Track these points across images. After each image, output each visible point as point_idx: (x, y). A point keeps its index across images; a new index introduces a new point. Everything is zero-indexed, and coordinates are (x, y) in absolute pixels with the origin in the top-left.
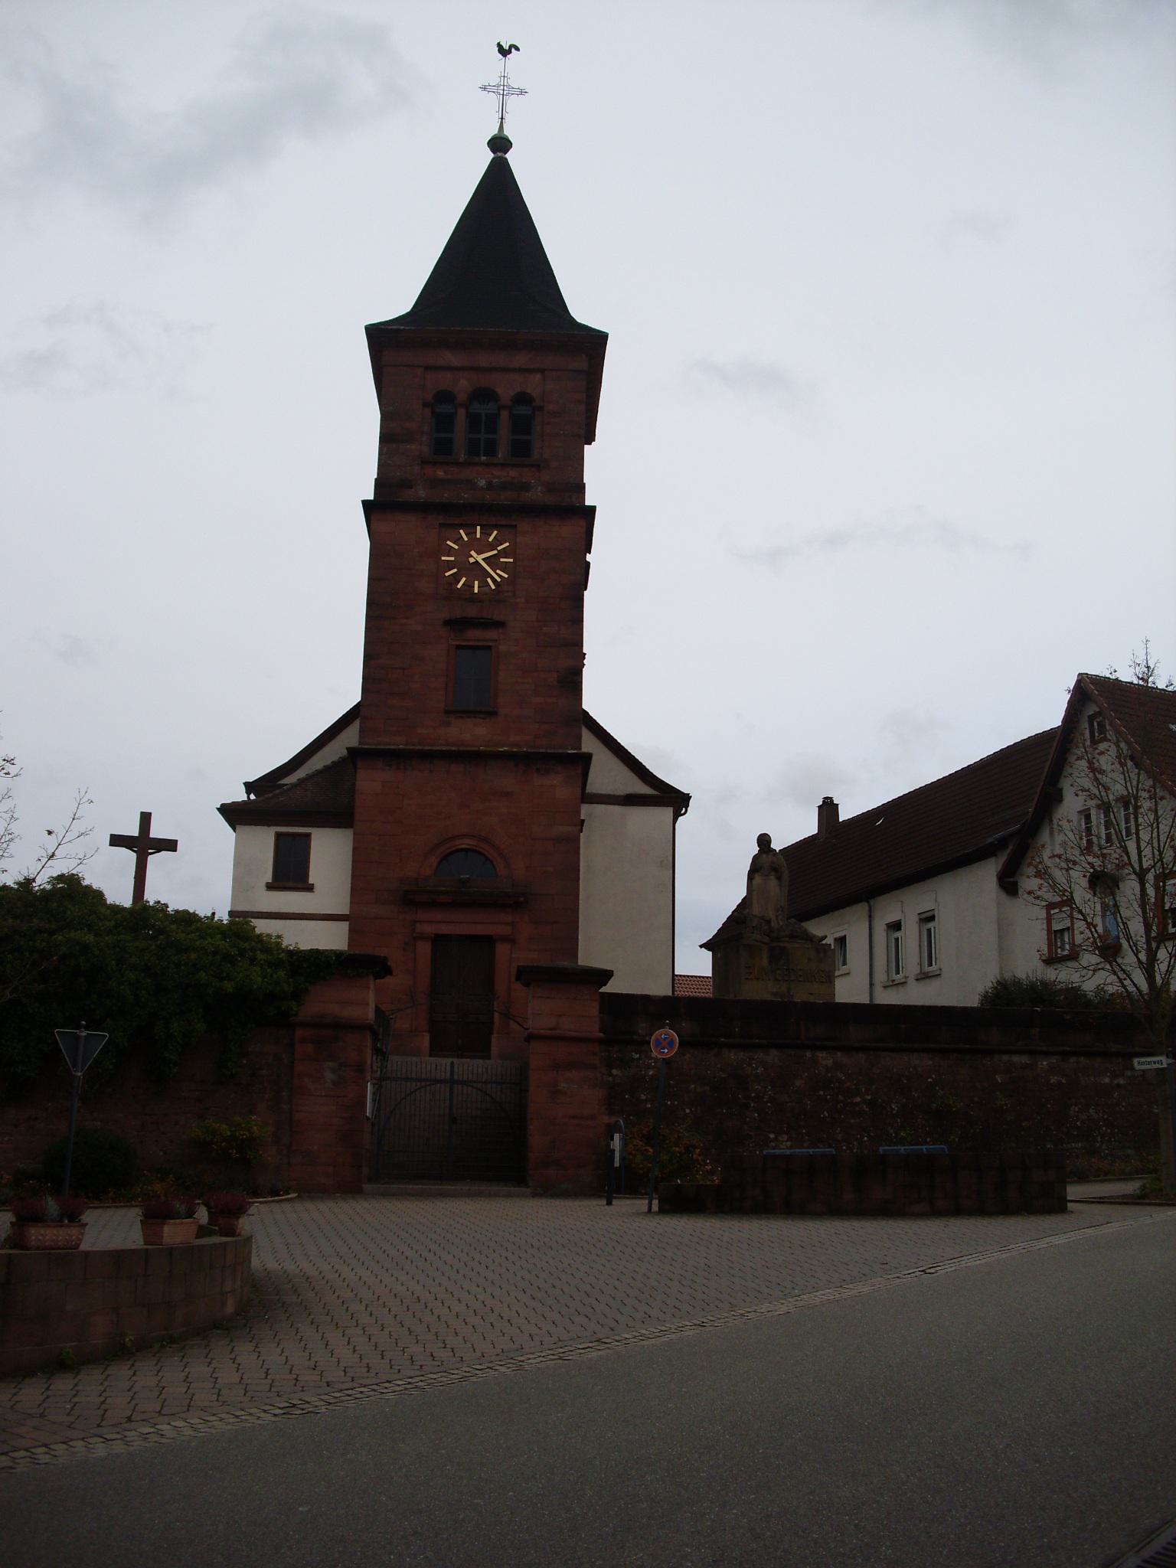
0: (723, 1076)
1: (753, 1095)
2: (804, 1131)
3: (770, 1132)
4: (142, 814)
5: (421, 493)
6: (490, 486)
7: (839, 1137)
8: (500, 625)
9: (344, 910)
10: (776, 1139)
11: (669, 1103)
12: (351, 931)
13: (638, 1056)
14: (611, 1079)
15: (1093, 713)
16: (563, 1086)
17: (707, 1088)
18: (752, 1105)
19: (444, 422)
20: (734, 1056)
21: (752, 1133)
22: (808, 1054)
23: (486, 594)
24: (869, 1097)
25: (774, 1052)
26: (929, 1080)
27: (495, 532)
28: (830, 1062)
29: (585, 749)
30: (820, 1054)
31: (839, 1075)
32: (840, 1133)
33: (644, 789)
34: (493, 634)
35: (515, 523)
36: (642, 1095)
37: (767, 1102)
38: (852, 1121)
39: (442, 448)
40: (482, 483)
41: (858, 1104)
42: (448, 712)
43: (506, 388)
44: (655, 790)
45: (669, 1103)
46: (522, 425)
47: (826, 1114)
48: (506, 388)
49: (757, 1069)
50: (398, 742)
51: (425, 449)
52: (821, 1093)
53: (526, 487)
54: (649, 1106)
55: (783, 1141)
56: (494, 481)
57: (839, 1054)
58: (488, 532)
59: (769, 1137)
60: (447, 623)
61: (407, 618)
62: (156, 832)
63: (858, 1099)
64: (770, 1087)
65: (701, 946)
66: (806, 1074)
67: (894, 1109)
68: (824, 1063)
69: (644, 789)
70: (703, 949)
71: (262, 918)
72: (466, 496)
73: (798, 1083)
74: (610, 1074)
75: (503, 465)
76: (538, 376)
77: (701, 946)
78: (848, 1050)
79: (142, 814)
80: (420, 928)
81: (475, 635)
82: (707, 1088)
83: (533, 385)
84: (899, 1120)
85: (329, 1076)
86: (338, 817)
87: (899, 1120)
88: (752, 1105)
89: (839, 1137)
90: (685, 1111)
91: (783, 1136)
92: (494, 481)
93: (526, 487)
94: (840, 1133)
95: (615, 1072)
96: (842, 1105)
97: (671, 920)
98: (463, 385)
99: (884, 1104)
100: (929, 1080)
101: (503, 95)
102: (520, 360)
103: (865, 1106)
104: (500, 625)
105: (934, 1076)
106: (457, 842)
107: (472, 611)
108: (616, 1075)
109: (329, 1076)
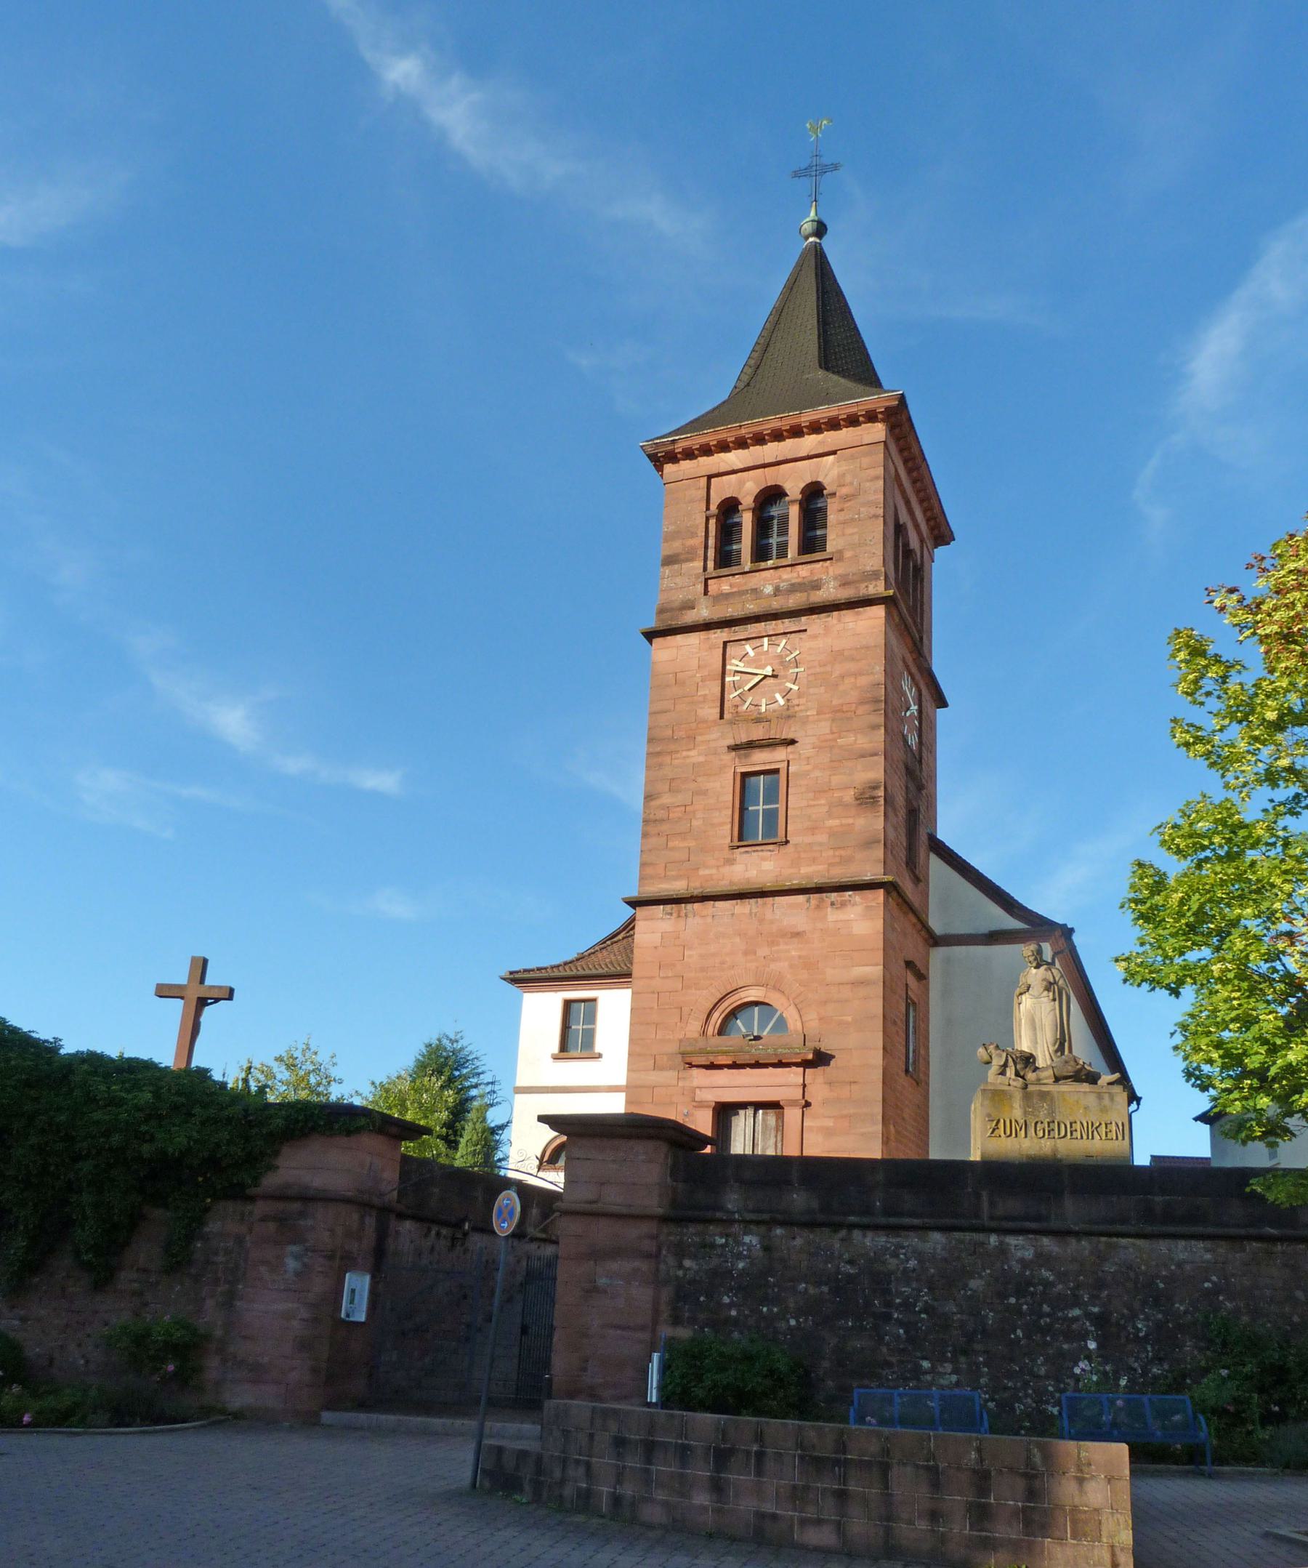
0: (852, 1271)
1: (898, 1301)
2: (981, 1359)
3: (925, 1358)
5: (704, 612)
6: (777, 591)
7: (1043, 1371)
9: (622, 1080)
10: (933, 1370)
11: (765, 1309)
13: (724, 1240)
14: (680, 1273)
16: (602, 1281)
17: (825, 1289)
18: (896, 1316)
20: (870, 1242)
21: (894, 1360)
22: (993, 1239)
23: (774, 711)
24: (1096, 1310)
25: (936, 1236)
26: (1206, 1285)
27: (784, 641)
28: (1029, 1254)
30: (1012, 1241)
31: (1046, 1273)
32: (1042, 1365)
33: (1011, 923)
34: (781, 754)
36: (725, 1297)
37: (920, 1312)
38: (1065, 1346)
39: (726, 558)
40: (769, 589)
41: (1076, 1319)
43: (793, 481)
44: (1026, 923)
45: (765, 1309)
47: (1019, 1333)
48: (793, 481)
49: (907, 1261)
50: (677, 887)
52: (1013, 1300)
53: (816, 586)
54: (734, 1313)
55: (945, 1374)
56: (782, 585)
57: (1046, 1241)
58: (776, 642)
59: (921, 1366)
60: (735, 748)
61: (689, 750)
62: (180, 976)
63: (1076, 1312)
64: (926, 1290)
65: (1196, 1119)
66: (988, 1271)
67: (1140, 1330)
68: (1019, 1254)
69: (1011, 923)
70: (1199, 1122)
71: (548, 1092)
72: (752, 607)
73: (975, 1284)
74: (681, 1266)
76: (831, 458)
77: (1196, 1119)
78: (1061, 1234)
80: (701, 1095)
82: (825, 1289)
83: (828, 472)
84: (1149, 1349)
85: (292, 1264)
86: (620, 976)
87: (1149, 1349)
88: (896, 1316)
89: (1043, 1371)
90: (788, 1322)
91: (946, 1365)
92: (782, 585)
94: (1042, 1365)
95: (687, 1263)
96: (1048, 1320)
97: (167, 995)
98: (747, 489)
99: (1122, 1322)
100: (1206, 1285)
102: (809, 443)
103: (1088, 1324)
105: (1214, 1278)
106: (742, 995)
107: (758, 733)
108: (689, 1269)
109: (292, 1264)
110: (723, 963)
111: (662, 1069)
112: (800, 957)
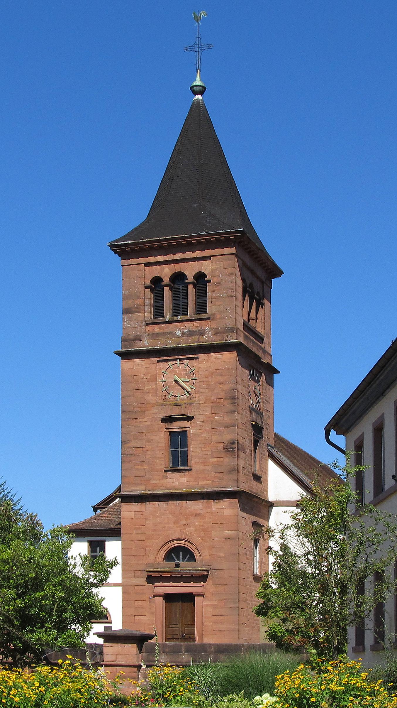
4: (94, 635)
5: (145, 344)
6: (183, 334)
8: (190, 418)
12: (124, 593)
15: (139, 503)
19: (158, 297)
29: (393, 482)
34: (187, 424)
35: (196, 356)
40: (179, 333)
42: (166, 471)
46: (202, 293)
51: (147, 315)
53: (202, 333)
75: (191, 320)
79: (94, 635)
81: (178, 425)
83: (206, 267)
93: (202, 333)
101: (198, 44)
104: (190, 418)
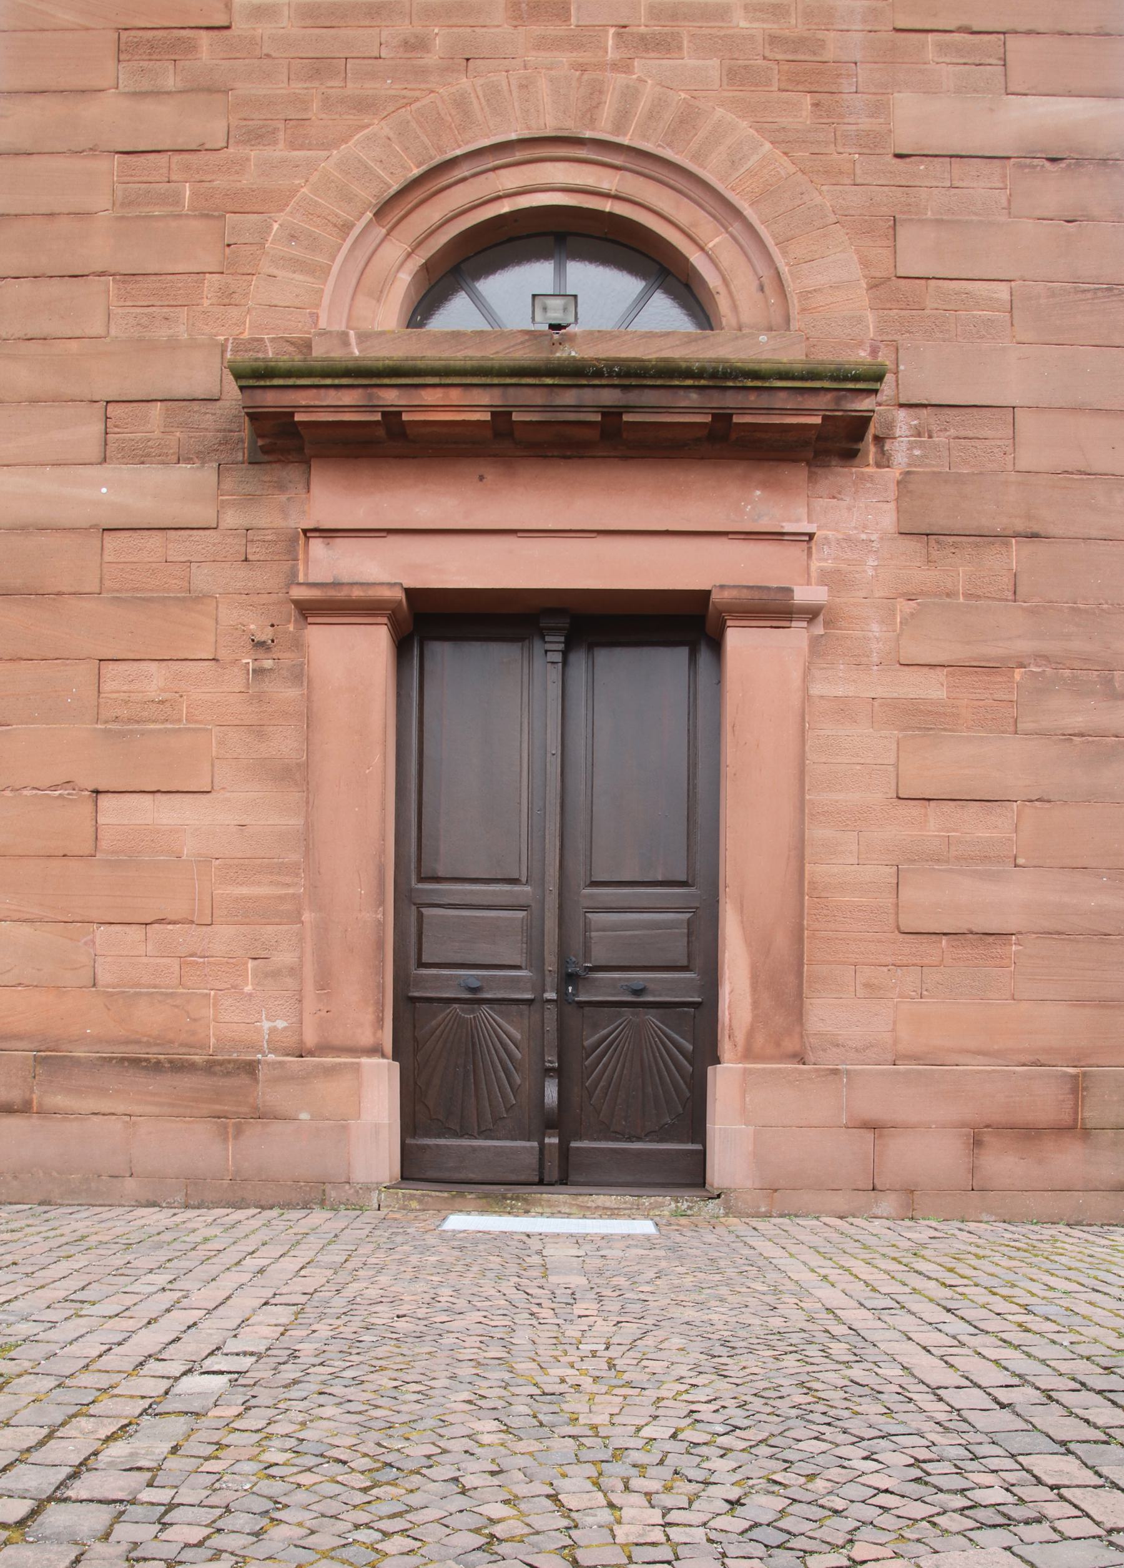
110: (416, 45)
111: (140, 456)
112: (774, 40)
